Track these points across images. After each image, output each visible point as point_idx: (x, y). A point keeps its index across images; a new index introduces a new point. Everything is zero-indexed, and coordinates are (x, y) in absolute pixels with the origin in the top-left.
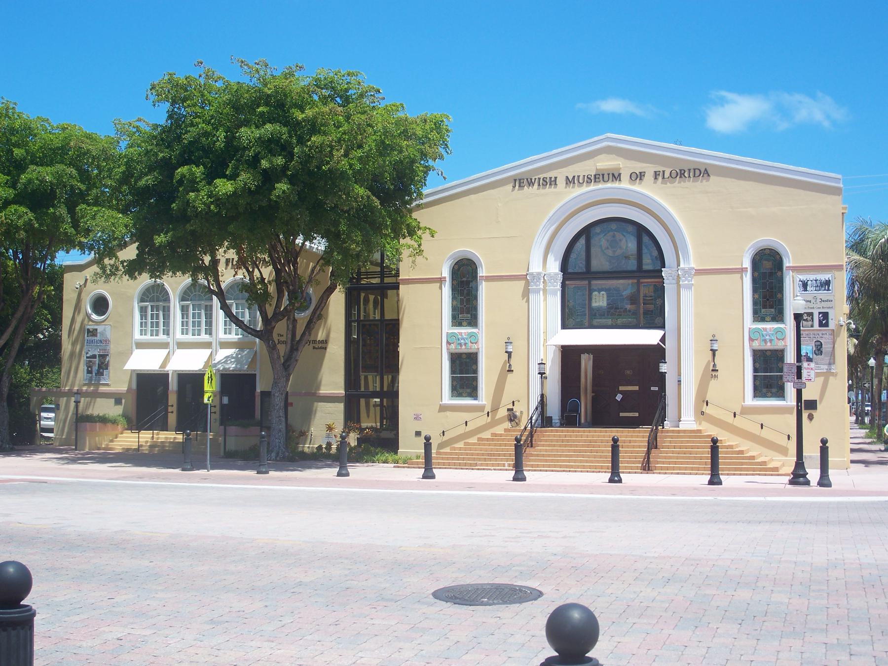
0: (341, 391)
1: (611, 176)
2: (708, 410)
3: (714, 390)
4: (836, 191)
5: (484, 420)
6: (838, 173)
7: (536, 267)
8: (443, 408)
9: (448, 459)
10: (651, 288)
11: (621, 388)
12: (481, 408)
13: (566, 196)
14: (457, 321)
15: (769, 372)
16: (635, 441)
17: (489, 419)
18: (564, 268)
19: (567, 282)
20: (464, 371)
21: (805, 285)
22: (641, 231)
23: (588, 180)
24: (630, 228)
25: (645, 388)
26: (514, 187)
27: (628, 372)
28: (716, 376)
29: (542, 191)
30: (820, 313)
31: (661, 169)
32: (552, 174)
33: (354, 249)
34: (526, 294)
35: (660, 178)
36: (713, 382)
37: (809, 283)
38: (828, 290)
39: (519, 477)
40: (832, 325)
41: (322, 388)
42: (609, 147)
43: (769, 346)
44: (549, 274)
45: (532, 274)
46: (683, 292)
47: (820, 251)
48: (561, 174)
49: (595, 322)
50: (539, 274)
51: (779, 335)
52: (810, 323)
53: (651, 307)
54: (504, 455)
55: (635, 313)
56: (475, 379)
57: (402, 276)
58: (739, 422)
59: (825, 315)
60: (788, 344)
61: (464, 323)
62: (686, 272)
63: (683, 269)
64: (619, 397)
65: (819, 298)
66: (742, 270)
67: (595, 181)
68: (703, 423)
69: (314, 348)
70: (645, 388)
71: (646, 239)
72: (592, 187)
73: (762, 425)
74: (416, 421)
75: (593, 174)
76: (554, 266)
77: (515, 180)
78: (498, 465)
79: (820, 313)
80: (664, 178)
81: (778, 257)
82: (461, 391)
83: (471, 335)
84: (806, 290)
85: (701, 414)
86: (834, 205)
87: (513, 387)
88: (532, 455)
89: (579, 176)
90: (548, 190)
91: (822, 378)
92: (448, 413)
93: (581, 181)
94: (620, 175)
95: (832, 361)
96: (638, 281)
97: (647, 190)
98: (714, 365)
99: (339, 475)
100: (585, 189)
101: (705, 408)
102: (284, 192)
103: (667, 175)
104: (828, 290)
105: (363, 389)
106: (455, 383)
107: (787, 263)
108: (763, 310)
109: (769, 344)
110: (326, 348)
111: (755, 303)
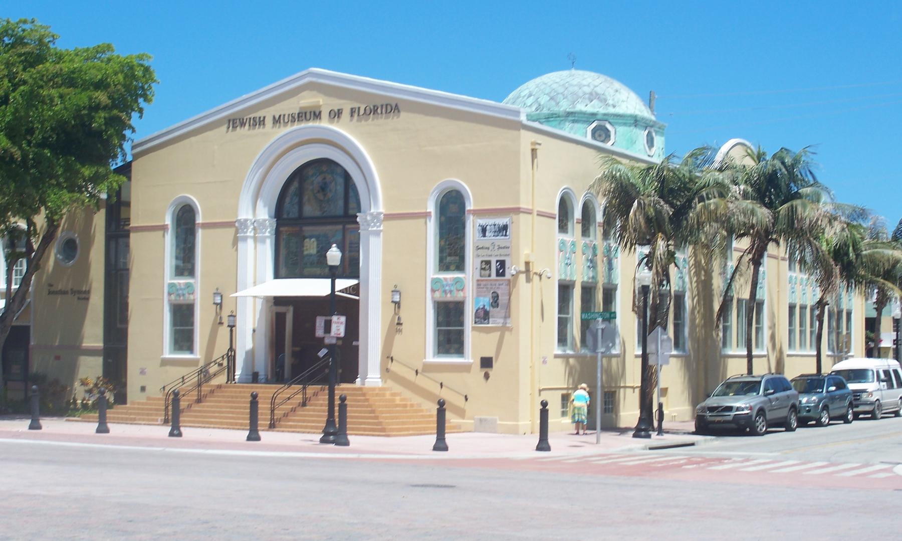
0: (100, 344)
2: (394, 367)
7: (245, 213)
8: (165, 362)
14: (444, 266)
19: (282, 229)
21: (484, 230)
28: (400, 331)
29: (252, 132)
30: (497, 261)
31: (356, 105)
36: (398, 337)
38: (506, 235)
41: (85, 340)
48: (269, 113)
52: (488, 272)
57: (133, 224)
58: (421, 381)
59: (502, 264)
60: (467, 295)
61: (186, 273)
63: (372, 214)
65: (497, 244)
69: (79, 299)
72: (296, 126)
73: (441, 384)
75: (297, 112)
76: (264, 213)
77: (229, 121)
79: (497, 261)
84: (484, 236)
85: (386, 372)
90: (258, 130)
91: (499, 333)
92: (168, 368)
94: (320, 113)
97: (343, 130)
99: (31, 428)
100: (289, 128)
104: (506, 235)
110: (88, 299)
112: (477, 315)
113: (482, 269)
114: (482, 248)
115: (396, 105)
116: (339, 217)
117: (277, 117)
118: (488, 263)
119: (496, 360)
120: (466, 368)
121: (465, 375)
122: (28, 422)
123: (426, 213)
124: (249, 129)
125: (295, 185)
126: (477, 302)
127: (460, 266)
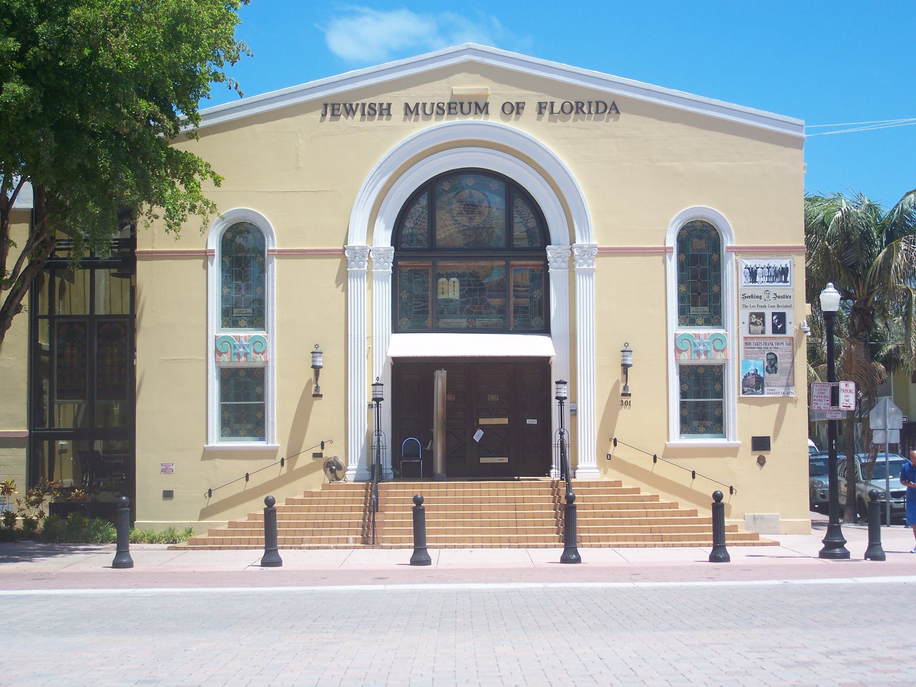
1: (473, 106)
2: (616, 452)
3: (626, 423)
4: (797, 143)
5: (275, 471)
6: (801, 118)
7: (357, 240)
8: (210, 454)
9: (243, 533)
10: (527, 275)
11: (482, 421)
12: (270, 454)
13: (403, 134)
14: (230, 318)
15: (702, 399)
16: (531, 500)
17: (284, 470)
18: (396, 240)
19: (399, 263)
20: (243, 398)
22: (514, 192)
23: (440, 110)
24: (495, 185)
25: (517, 421)
26: (324, 115)
27: (493, 398)
28: (628, 404)
29: (368, 124)
30: (774, 314)
31: (548, 99)
32: (384, 99)
33: (127, 197)
34: (343, 278)
35: (547, 113)
36: (623, 412)
37: (759, 270)
39: (570, 556)
40: (791, 330)
42: (471, 63)
43: (703, 360)
44: (378, 250)
45: (353, 248)
46: (581, 282)
47: (765, 226)
48: (397, 100)
49: (442, 323)
50: (363, 249)
51: (718, 345)
52: (760, 328)
53: (524, 302)
54: (340, 525)
55: (502, 311)
56: (262, 409)
58: (662, 469)
59: (781, 318)
60: (730, 357)
62: (584, 251)
63: (581, 247)
64: (478, 435)
65: (772, 291)
66: (665, 251)
67: (449, 113)
68: (610, 470)
70: (517, 421)
71: (519, 202)
72: (445, 121)
73: (694, 473)
74: (165, 475)
76: (383, 238)
77: (326, 105)
78: (338, 541)
79: (774, 314)
80: (552, 112)
81: (713, 233)
82: (237, 426)
83: (256, 341)
86: (790, 165)
87: (323, 421)
88: (385, 524)
89: (424, 104)
90: (377, 123)
91: (778, 405)
92: (218, 462)
93: (428, 112)
94: (487, 105)
95: (790, 381)
96: (507, 263)
97: (528, 130)
98: (625, 388)
101: (612, 450)
102: (17, 97)
103: (557, 108)
104: (786, 281)
105: (47, 426)
106: (226, 415)
107: (728, 242)
108: (692, 309)
109: (703, 357)
111: (681, 298)
112: (745, 383)
113: (752, 323)
114: (752, 296)
115: (614, 104)
116: (501, 250)
117: (412, 106)
118: (761, 316)
119: (775, 439)
120: (732, 451)
121: (729, 459)
122: (109, 552)
123: (665, 249)
124: (362, 120)
125: (423, 201)
126: (745, 367)
127: (715, 317)
